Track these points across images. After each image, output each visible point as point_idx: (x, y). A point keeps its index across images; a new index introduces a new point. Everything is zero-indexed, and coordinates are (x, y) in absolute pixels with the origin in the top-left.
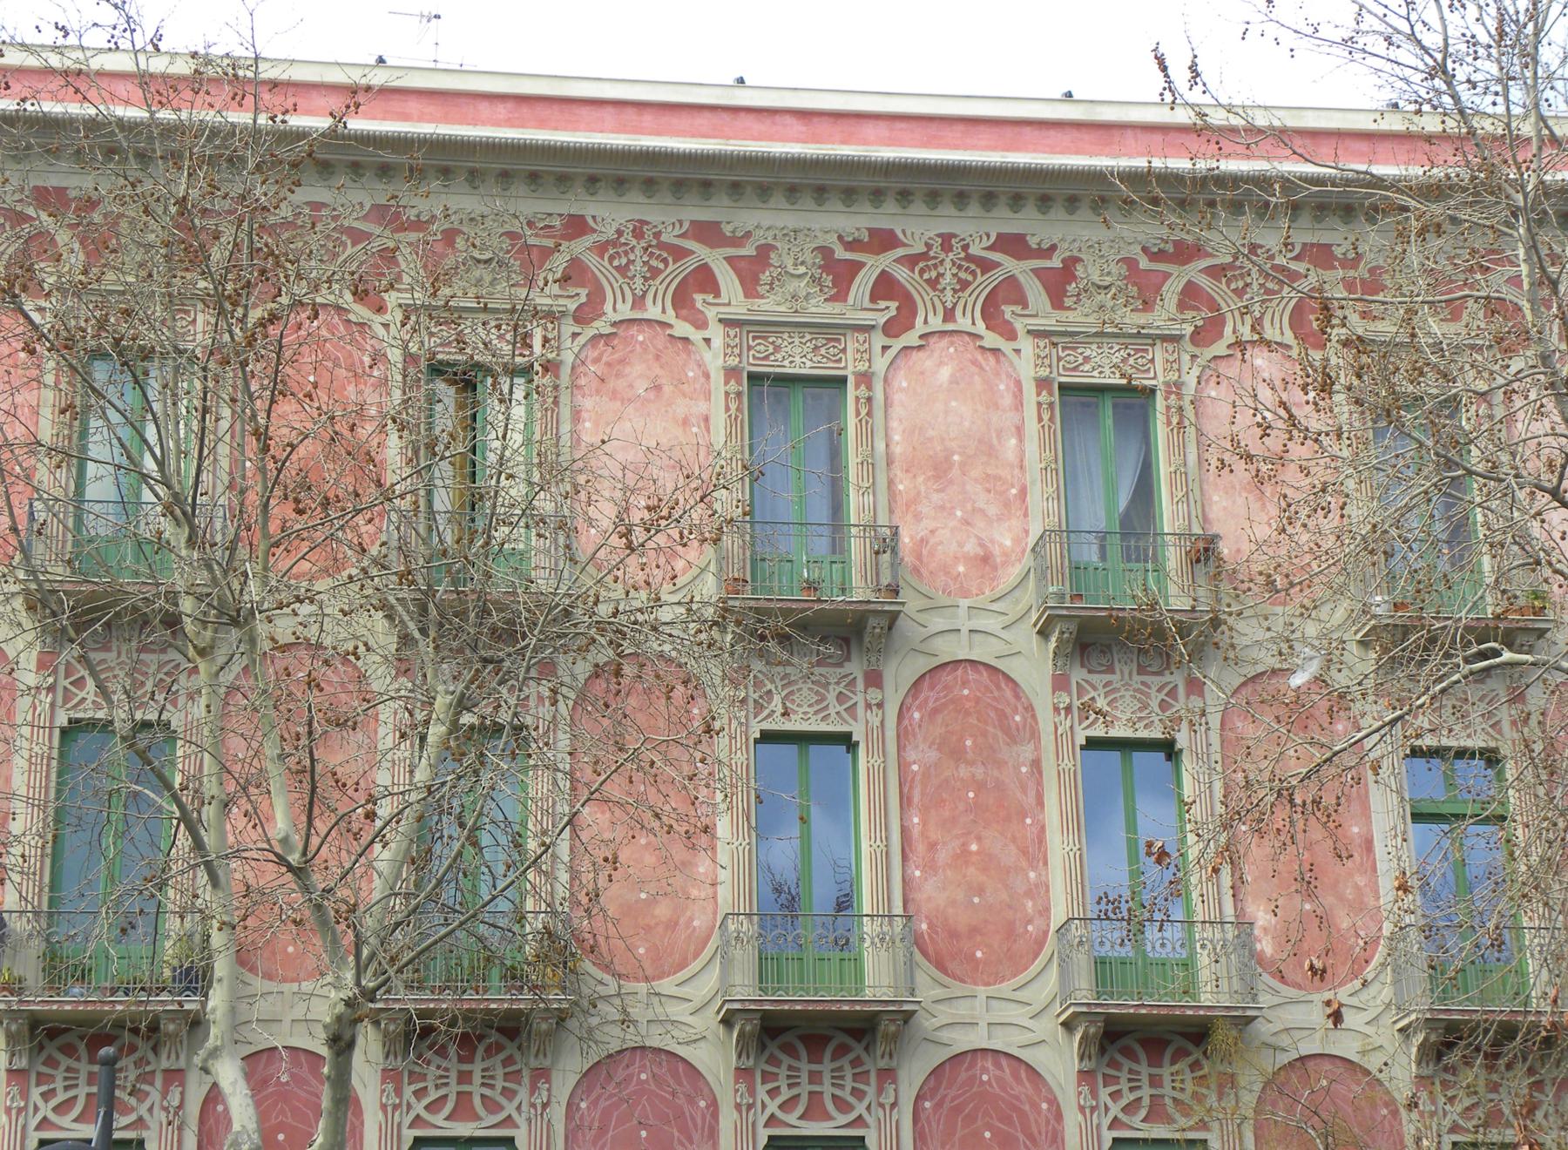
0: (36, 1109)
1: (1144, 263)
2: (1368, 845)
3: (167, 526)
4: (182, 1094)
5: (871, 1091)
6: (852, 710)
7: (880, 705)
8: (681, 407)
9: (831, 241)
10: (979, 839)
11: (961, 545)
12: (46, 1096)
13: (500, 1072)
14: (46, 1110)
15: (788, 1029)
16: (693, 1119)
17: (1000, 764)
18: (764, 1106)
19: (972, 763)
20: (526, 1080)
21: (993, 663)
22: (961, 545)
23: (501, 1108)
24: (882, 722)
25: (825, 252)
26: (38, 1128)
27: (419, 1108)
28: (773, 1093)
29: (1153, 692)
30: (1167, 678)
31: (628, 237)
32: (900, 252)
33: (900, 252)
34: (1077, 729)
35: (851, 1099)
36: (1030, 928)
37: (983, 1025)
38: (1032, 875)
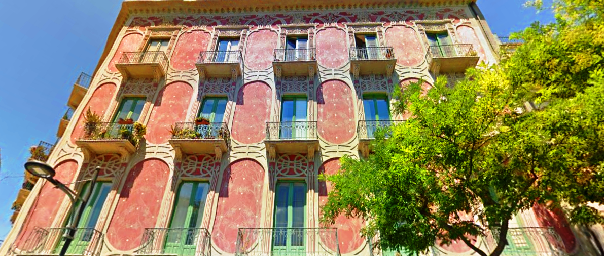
0: (277, 172)
1: (372, 15)
2: (270, 113)
3: (410, 57)
4: (314, 167)
5: (307, 168)
6: (306, 89)
7: (313, 88)
8: (271, 41)
9: (370, 13)
10: (337, 114)
11: (332, 59)
12: (185, 169)
13: (301, 164)
14: (279, 172)
15: (102, 154)
16: (258, 175)
17: (341, 98)
18: (277, 172)
19: (335, 98)
20: (214, 166)
21: (187, 81)
22: (332, 59)
23: (301, 172)
24: (234, 92)
25: (369, 16)
26: (277, 176)
27: (184, 172)
28: (280, 169)
29: (380, 83)
30: (383, 80)
31: (264, 17)
32: (386, 14)
33: (386, 14)
34: (361, 91)
35: (301, 170)
36: (350, 131)
37: (338, 152)
38: (350, 120)
